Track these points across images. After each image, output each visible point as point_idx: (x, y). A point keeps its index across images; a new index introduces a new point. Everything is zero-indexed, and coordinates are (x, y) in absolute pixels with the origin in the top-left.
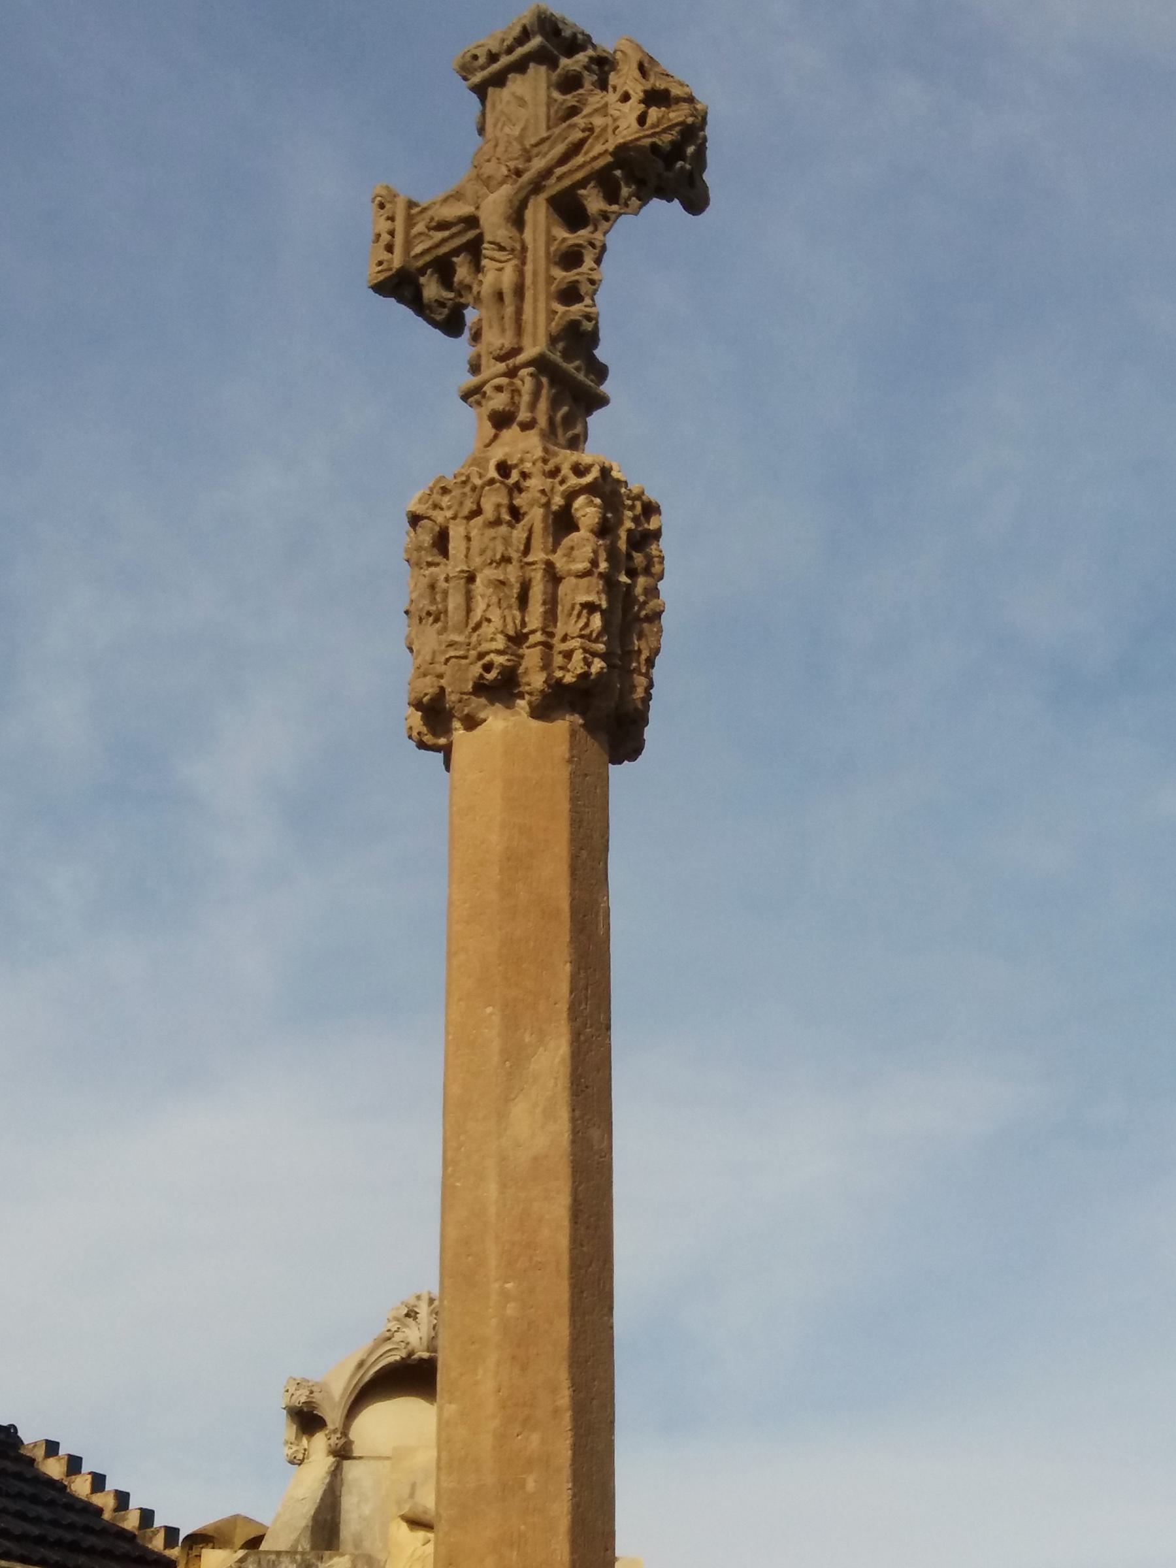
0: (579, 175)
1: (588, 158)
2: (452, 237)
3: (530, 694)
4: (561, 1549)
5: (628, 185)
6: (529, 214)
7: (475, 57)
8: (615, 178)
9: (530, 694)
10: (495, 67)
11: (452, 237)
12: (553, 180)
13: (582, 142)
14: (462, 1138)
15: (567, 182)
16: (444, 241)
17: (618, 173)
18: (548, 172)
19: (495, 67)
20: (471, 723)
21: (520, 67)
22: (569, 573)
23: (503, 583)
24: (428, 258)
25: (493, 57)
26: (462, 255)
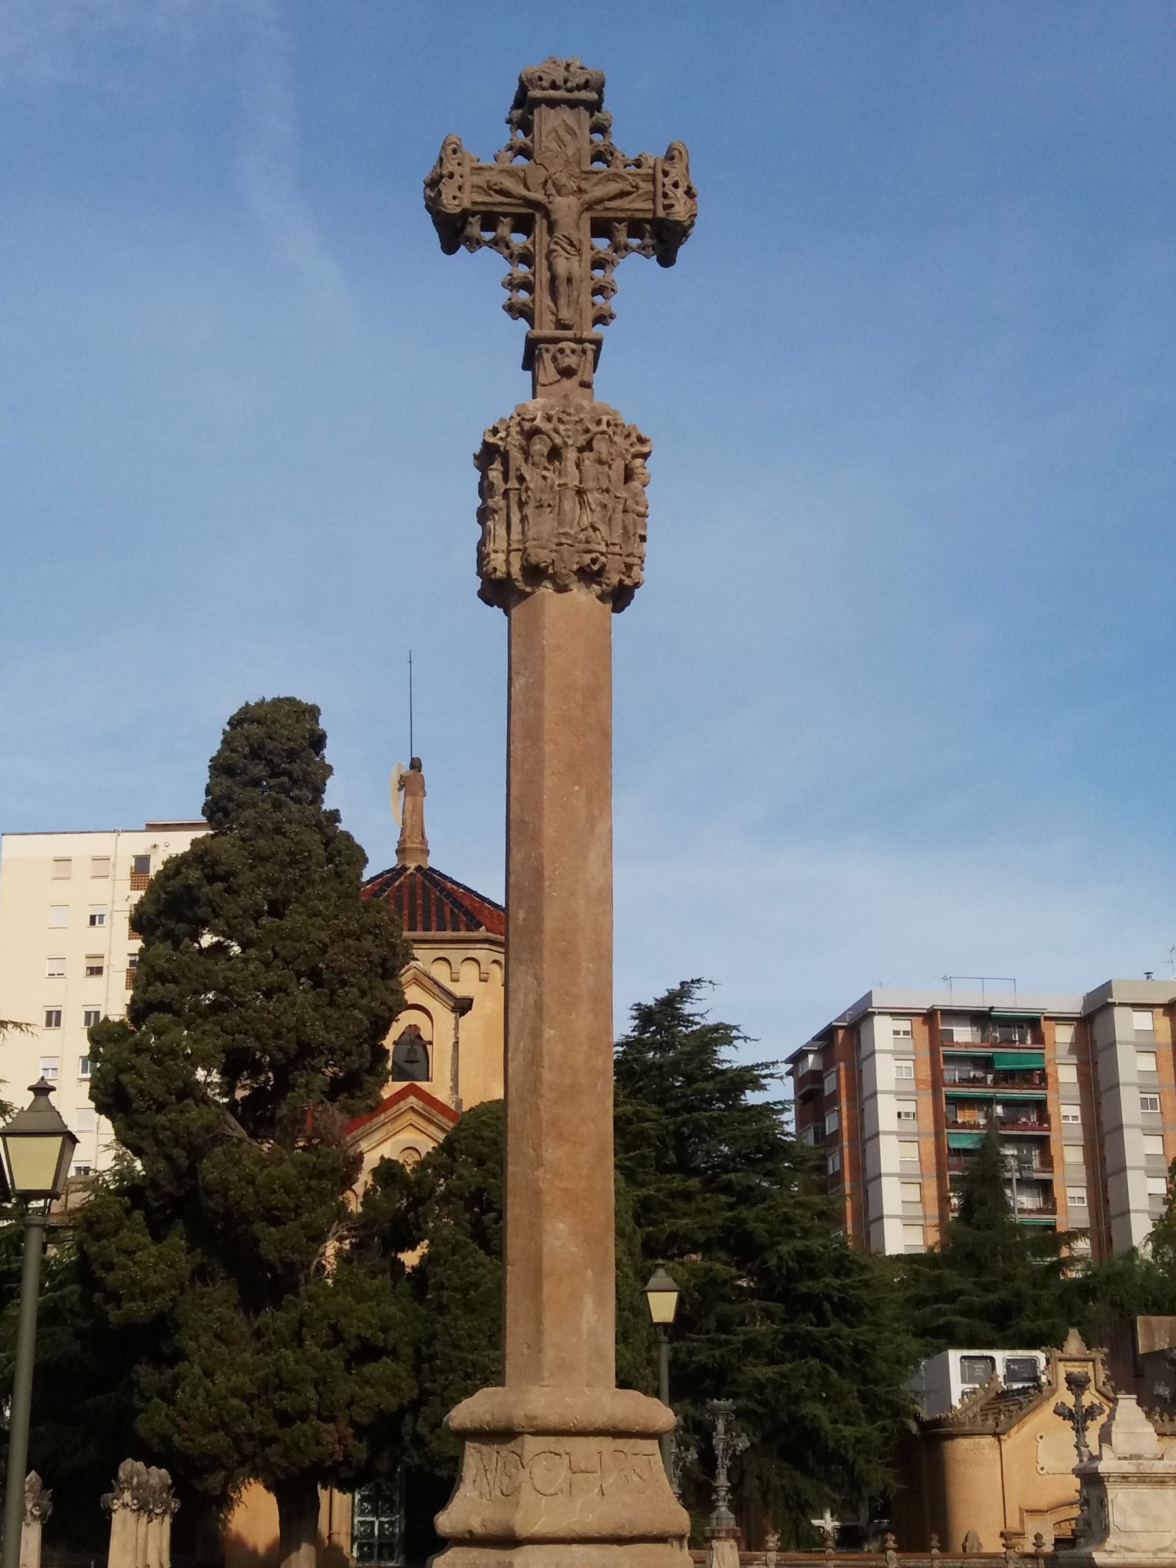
0: (621, 215)
1: (628, 206)
2: (516, 205)
3: (607, 585)
4: (1168, 1493)
5: (651, 238)
6: (581, 225)
7: (540, 79)
8: (645, 228)
9: (607, 585)
10: (552, 93)
11: (509, 204)
12: (599, 207)
13: (628, 194)
14: (557, 865)
15: (610, 214)
16: (502, 204)
17: (648, 227)
18: (600, 201)
19: (552, 93)
20: (562, 589)
21: (573, 104)
22: (633, 511)
23: (605, 506)
24: (483, 208)
25: (554, 86)
26: (508, 219)
